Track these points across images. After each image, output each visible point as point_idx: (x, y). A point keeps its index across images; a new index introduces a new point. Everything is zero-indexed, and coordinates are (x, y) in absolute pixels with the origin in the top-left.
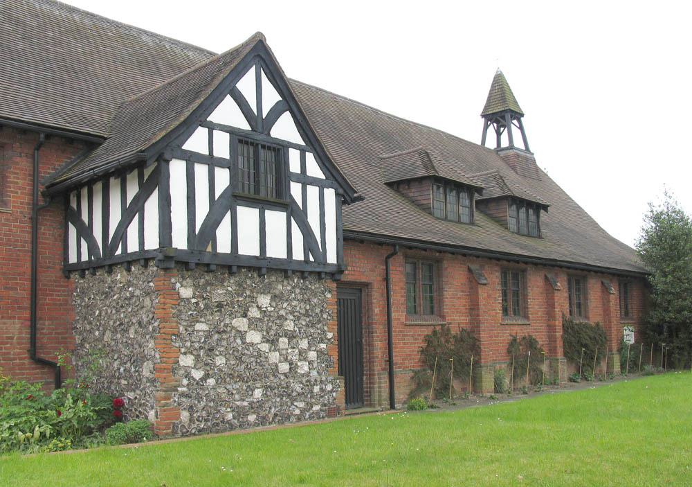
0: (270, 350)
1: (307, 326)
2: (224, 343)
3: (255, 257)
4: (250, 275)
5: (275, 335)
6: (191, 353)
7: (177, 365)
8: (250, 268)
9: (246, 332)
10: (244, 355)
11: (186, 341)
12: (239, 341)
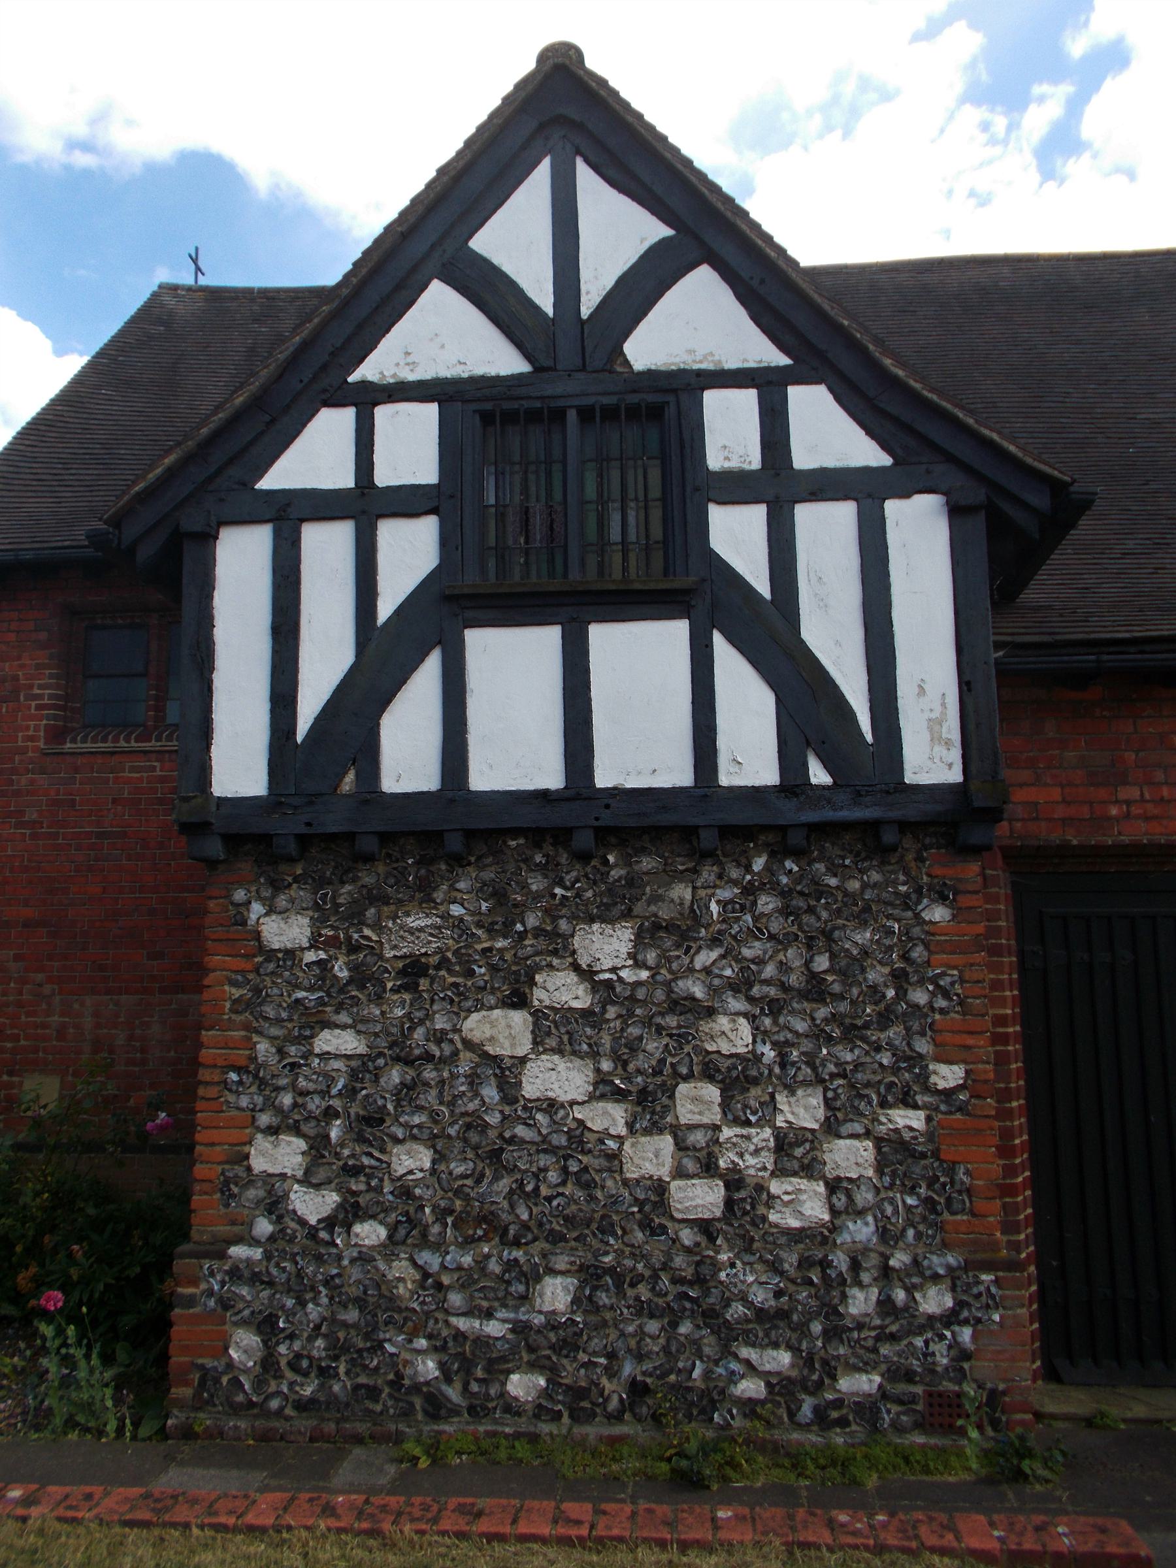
0: (630, 1126)
1: (819, 1035)
2: (430, 1098)
3: (543, 795)
4: (539, 858)
5: (657, 1072)
6: (296, 1131)
7: (239, 1170)
8: (536, 836)
9: (523, 1060)
10: (512, 1140)
11: (278, 1089)
12: (490, 1093)
